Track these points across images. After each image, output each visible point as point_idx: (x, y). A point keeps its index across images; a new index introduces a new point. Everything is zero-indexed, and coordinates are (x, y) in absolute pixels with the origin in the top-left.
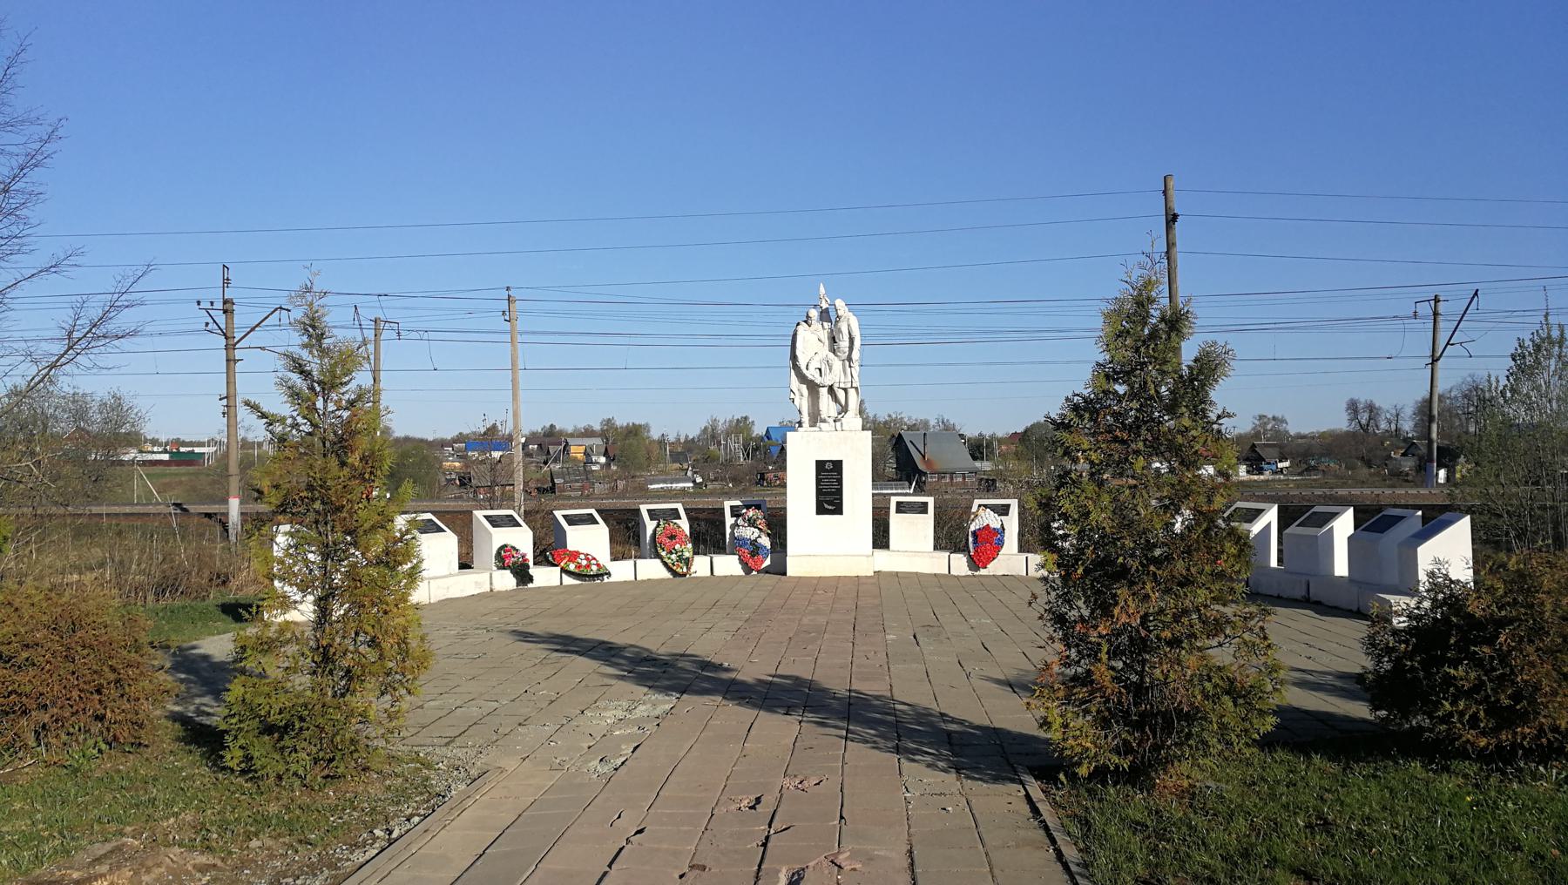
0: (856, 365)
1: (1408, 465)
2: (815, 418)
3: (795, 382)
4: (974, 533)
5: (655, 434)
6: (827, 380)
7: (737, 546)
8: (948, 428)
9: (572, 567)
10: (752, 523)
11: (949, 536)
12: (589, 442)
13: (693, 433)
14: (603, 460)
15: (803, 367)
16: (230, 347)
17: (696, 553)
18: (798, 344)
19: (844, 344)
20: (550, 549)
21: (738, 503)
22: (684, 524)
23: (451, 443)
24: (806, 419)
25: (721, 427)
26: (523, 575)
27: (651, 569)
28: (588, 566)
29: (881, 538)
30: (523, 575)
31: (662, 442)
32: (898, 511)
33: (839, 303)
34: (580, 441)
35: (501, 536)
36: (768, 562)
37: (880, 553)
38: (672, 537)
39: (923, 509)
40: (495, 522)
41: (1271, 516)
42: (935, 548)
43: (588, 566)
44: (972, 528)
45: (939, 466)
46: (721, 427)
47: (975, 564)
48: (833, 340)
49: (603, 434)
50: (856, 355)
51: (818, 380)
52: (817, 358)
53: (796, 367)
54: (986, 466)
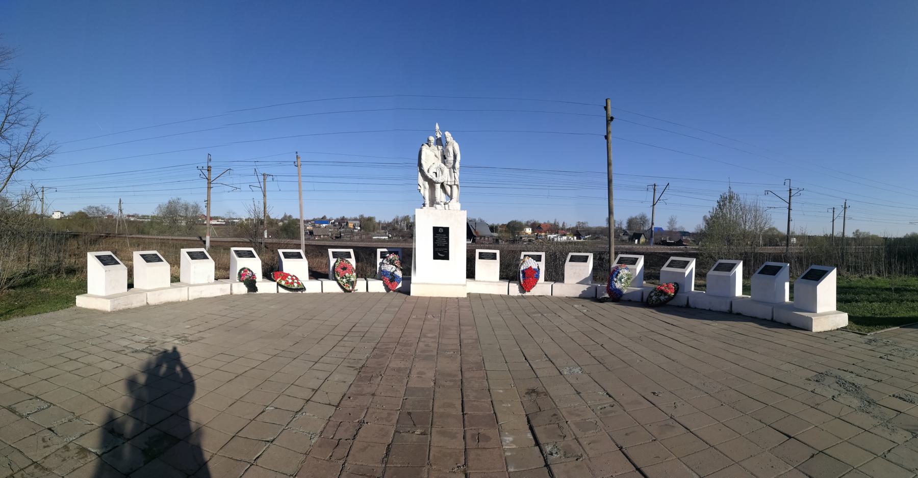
0: (457, 171)
1: (626, 238)
2: (433, 202)
3: (421, 180)
4: (523, 271)
5: (377, 220)
7: (380, 275)
8: (482, 222)
9: (283, 283)
10: (392, 262)
11: (508, 273)
13: (390, 220)
15: (426, 171)
16: (209, 183)
17: (357, 277)
18: (423, 157)
19: (451, 158)
20: (272, 271)
21: (385, 250)
22: (352, 261)
24: (427, 202)
25: (400, 219)
26: (251, 285)
27: (331, 287)
28: (292, 283)
30: (251, 285)
31: (379, 223)
33: (447, 134)
35: (242, 263)
36: (400, 285)
37: (470, 283)
38: (344, 269)
39: (493, 257)
40: (240, 254)
41: (692, 265)
42: (501, 278)
43: (292, 283)
44: (522, 268)
45: (480, 234)
46: (400, 219)
47: (523, 289)
48: (444, 158)
49: (360, 220)
50: (457, 165)
51: (435, 179)
52: (434, 166)
53: (422, 171)
54: (495, 234)
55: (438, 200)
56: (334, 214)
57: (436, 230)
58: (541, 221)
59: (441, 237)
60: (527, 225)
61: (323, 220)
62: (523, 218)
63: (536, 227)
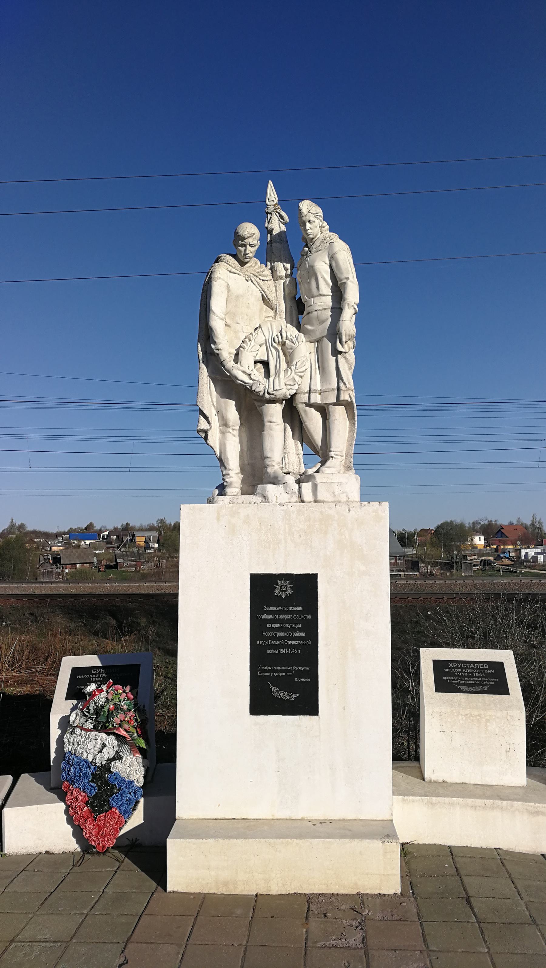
0: (348, 348)
2: (257, 475)
3: (208, 394)
6: (282, 385)
10: (103, 722)
12: (148, 534)
14: (156, 546)
15: (230, 363)
19: (322, 302)
23: (57, 535)
24: (235, 477)
29: (407, 746)
32: (442, 686)
34: (141, 533)
36: (137, 818)
48: (298, 309)
50: (348, 323)
51: (260, 383)
53: (213, 360)
55: (275, 466)
56: (108, 520)
57: (263, 587)
58: (503, 518)
59: (284, 609)
60: (475, 529)
61: (89, 531)
62: (466, 517)
63: (494, 533)
